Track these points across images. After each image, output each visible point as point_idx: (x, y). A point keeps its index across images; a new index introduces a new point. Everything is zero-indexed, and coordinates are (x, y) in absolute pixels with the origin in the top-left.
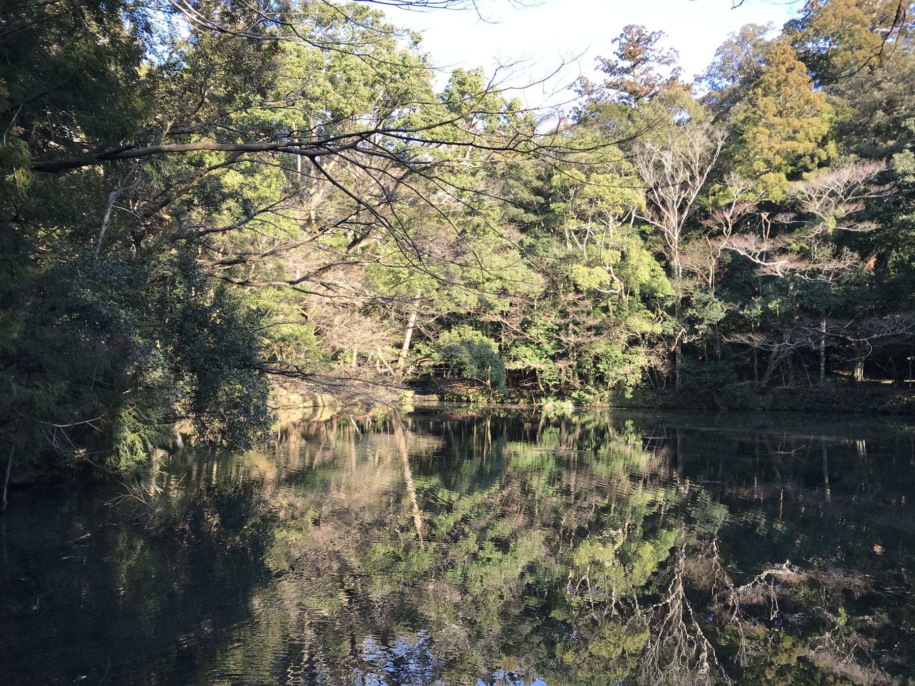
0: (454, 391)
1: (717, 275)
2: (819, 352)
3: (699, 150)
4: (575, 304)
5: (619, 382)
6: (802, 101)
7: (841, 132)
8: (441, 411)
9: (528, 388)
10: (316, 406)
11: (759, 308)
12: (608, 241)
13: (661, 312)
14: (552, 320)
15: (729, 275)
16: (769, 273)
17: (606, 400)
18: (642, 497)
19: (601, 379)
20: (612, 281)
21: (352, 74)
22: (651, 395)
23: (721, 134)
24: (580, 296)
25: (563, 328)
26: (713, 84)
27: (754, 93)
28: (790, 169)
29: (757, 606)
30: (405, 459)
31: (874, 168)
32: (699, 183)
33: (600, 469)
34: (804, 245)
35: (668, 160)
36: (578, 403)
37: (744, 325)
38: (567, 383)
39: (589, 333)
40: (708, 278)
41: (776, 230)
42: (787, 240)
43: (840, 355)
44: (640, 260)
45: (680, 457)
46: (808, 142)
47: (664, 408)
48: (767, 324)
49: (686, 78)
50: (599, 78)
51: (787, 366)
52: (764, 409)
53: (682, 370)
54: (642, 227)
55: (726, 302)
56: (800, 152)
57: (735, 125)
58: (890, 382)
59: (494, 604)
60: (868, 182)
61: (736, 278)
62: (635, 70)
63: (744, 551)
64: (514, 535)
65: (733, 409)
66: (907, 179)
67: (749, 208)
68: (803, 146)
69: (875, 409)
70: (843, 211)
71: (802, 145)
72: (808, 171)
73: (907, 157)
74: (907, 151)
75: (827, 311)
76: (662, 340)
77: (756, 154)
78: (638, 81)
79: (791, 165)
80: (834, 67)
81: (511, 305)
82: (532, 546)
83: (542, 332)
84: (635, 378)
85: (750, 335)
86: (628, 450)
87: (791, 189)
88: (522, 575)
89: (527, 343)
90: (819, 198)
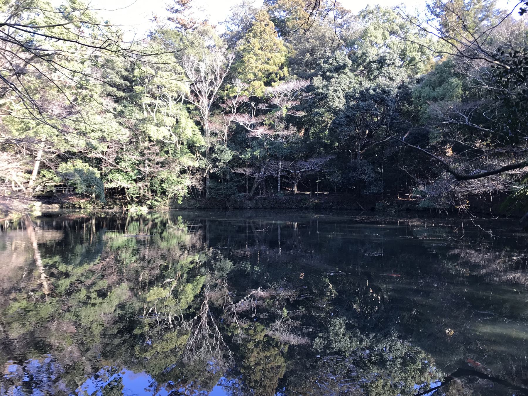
1: (228, 135)
3: (220, 64)
4: (149, 148)
5: (175, 195)
7: (290, 63)
8: (61, 215)
11: (249, 154)
12: (168, 112)
13: (198, 155)
14: (135, 157)
17: (167, 205)
18: (186, 259)
19: (164, 193)
22: (192, 202)
23: (231, 56)
24: (152, 143)
28: (266, 79)
30: (35, 245)
31: (305, 84)
32: (219, 82)
33: (163, 244)
34: (272, 122)
36: (151, 207)
38: (144, 196)
39: (157, 166)
41: (259, 112)
43: (287, 179)
45: (208, 235)
46: (274, 66)
47: (200, 209)
48: (253, 163)
51: (263, 185)
52: (251, 208)
53: (210, 188)
54: (188, 106)
55: (233, 150)
56: (271, 71)
58: (309, 193)
60: (302, 90)
61: (238, 137)
63: (239, 283)
66: (319, 90)
67: (245, 99)
68: (273, 68)
69: (302, 207)
71: (271, 67)
72: (275, 82)
75: (282, 157)
76: (199, 171)
77: (249, 69)
79: (266, 78)
82: (121, 293)
83: (129, 165)
84: (184, 192)
89: (119, 171)
90: (279, 97)
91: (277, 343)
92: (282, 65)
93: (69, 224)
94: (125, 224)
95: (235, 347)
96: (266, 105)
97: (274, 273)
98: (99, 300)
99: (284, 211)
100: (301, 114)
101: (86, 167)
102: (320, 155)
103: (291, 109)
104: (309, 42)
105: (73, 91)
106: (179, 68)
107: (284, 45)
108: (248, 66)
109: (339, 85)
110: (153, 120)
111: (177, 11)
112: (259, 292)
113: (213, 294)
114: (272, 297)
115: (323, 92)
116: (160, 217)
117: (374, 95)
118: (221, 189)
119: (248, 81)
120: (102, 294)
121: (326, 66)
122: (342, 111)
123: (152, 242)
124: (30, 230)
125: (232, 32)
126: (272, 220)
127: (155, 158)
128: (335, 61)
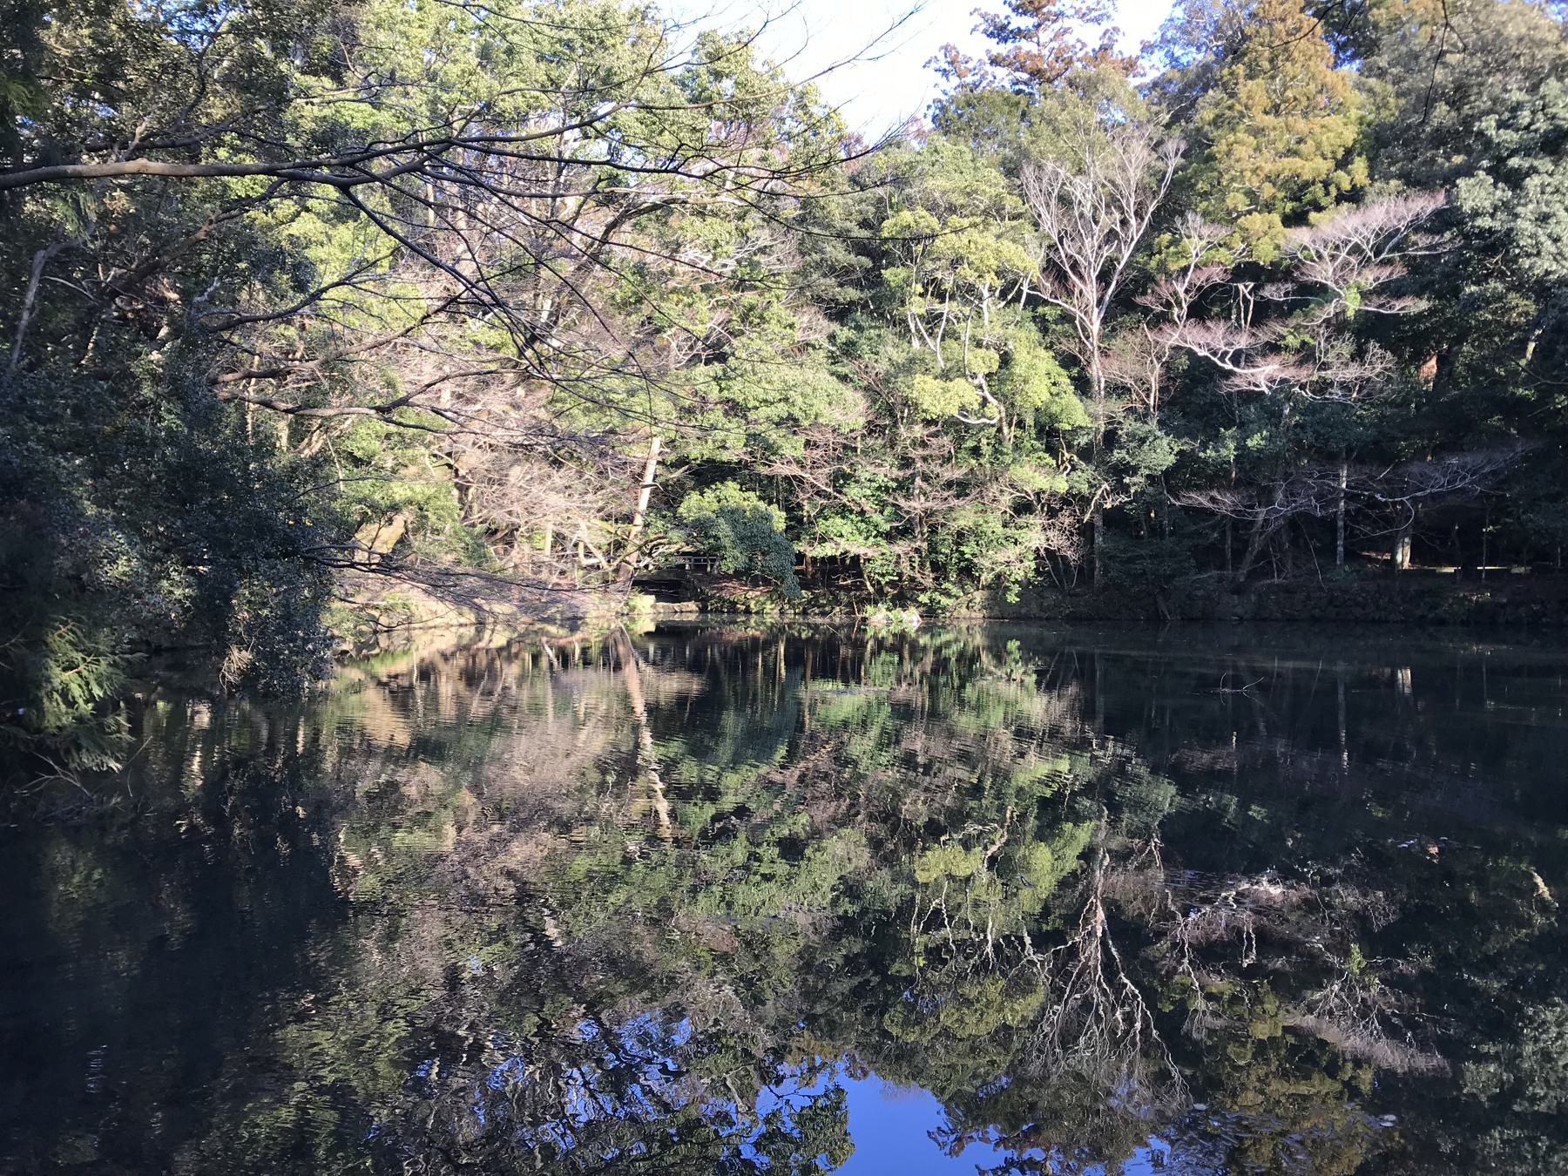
0: (725, 595)
1: (1162, 390)
2: (1334, 521)
3: (1135, 174)
4: (924, 444)
5: (998, 576)
6: (1312, 86)
7: (1378, 143)
8: (702, 630)
9: (847, 589)
10: (480, 625)
11: (1232, 446)
12: (979, 333)
13: (1067, 455)
14: (887, 472)
15: (1187, 390)
16: (1245, 387)
17: (977, 607)
18: (1035, 769)
19: (968, 572)
20: (985, 402)
21: (515, 39)
22: (1051, 598)
23: (1175, 144)
24: (933, 429)
25: (904, 486)
26: (1174, 59)
27: (1231, 74)
28: (1289, 206)
29: (1220, 943)
30: (640, 708)
31: (1425, 204)
32: (1136, 230)
33: (966, 722)
34: (1307, 338)
35: (1081, 190)
36: (930, 612)
37: (1214, 477)
38: (912, 579)
39: (946, 494)
40: (1148, 396)
41: (1263, 312)
42: (1279, 329)
43: (1372, 523)
44: (1032, 367)
45: (1100, 701)
46: (1319, 160)
47: (1074, 619)
48: (1251, 474)
49: (1127, 47)
50: (979, 47)
51: (1281, 545)
52: (1241, 619)
53: (1103, 553)
54: (1040, 310)
55: (1179, 436)
56: (1307, 176)
57: (1198, 130)
58: (1451, 570)
59: (783, 952)
60: (1416, 227)
61: (1194, 396)
62: (1040, 34)
63: (1201, 851)
64: (816, 834)
65: (1191, 620)
66: (1479, 222)
67: (1217, 275)
68: (1313, 167)
69: (1423, 617)
70: (1371, 278)
71: (1308, 165)
72: (1319, 209)
73: (1481, 183)
74: (1481, 174)
75: (1350, 450)
76: (1070, 504)
77: (1233, 180)
78: (1045, 52)
79: (1291, 200)
80: (1376, 26)
81: (807, 444)
82: (845, 851)
83: (869, 492)
84: (1023, 570)
85: (1214, 493)
86: (1011, 691)
87: (1288, 241)
88: (835, 902)
89: (843, 511)
90: (1333, 258)
91: (1335, 1056)
92: (1349, 152)
93: (723, 655)
94: (863, 654)
95: (1186, 1050)
96: (1289, 286)
97: (1306, 832)
98: (782, 868)
100: (1416, 305)
101: (750, 501)
103: (1371, 292)
104: (1445, 65)
105: (718, 297)
106: (1011, 203)
107: (1359, 87)
108: (1227, 171)
109: (1557, 197)
110: (935, 360)
111: (1019, 33)
112: (1270, 889)
113: (1118, 878)
114: (1309, 906)
115: (1497, 225)
116: (957, 640)
118: (1142, 557)
119: (1231, 218)
120: (792, 849)
121: (1509, 137)
123: (934, 714)
124: (629, 670)
125: (1183, 72)
126: (1316, 659)
127: (938, 470)
128: (1540, 115)
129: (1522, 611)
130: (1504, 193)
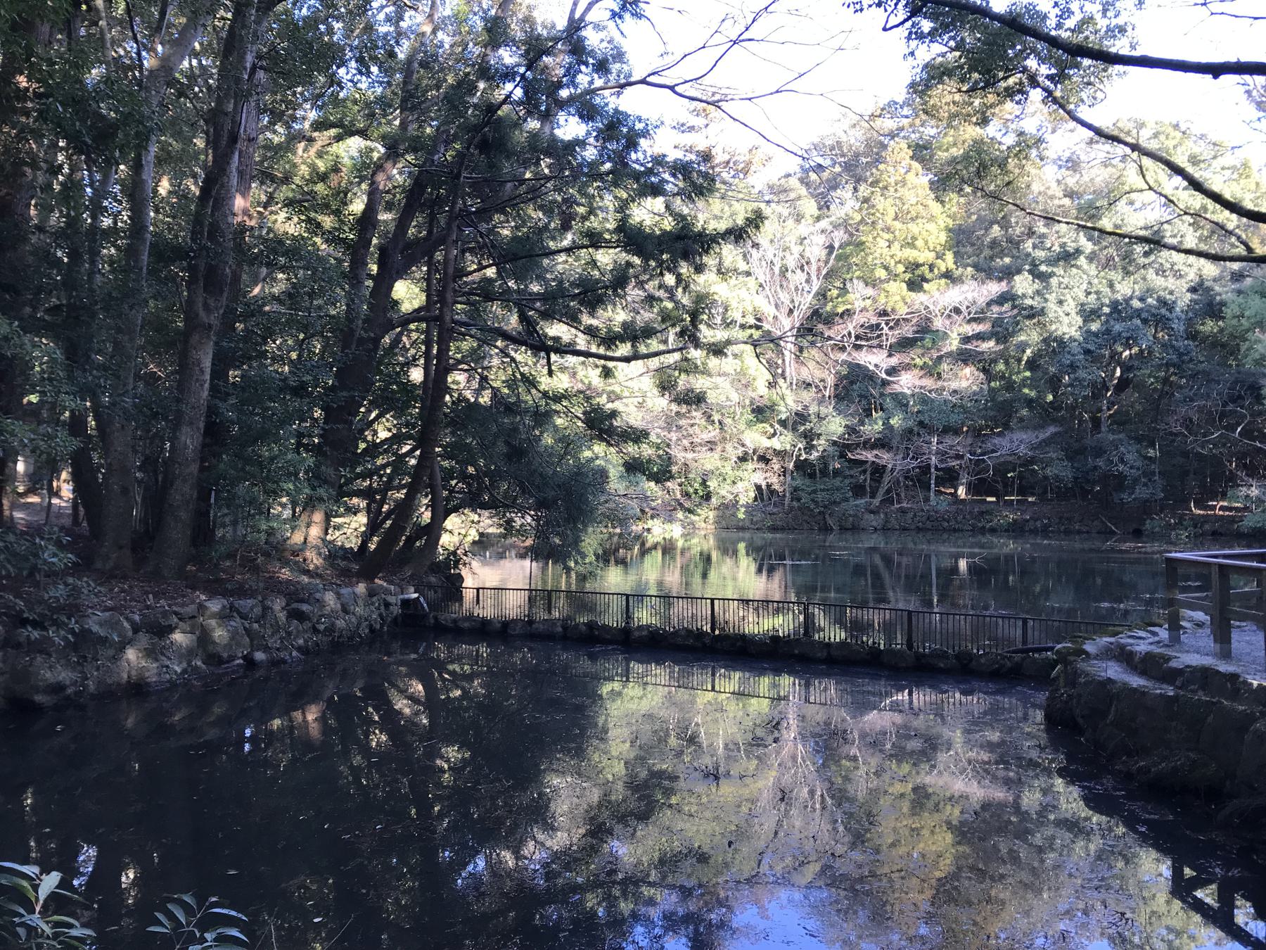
31: (995, 288)
56: (921, 262)
61: (856, 389)
68: (925, 256)
69: (984, 527)
72: (927, 281)
84: (746, 495)
99: (945, 536)
100: (989, 345)
102: (1024, 424)
111: (692, 128)
115: (1035, 303)
117: (1142, 309)
122: (1075, 340)
129: (1038, 524)
130: (1037, 285)
